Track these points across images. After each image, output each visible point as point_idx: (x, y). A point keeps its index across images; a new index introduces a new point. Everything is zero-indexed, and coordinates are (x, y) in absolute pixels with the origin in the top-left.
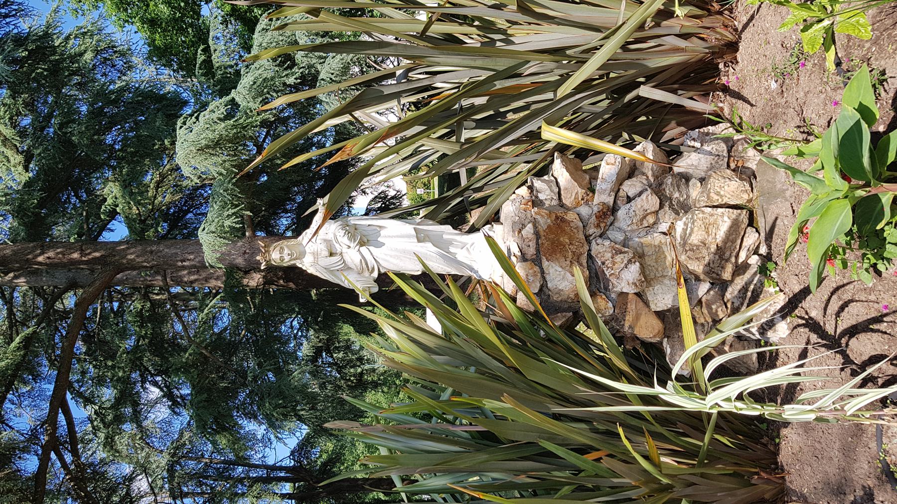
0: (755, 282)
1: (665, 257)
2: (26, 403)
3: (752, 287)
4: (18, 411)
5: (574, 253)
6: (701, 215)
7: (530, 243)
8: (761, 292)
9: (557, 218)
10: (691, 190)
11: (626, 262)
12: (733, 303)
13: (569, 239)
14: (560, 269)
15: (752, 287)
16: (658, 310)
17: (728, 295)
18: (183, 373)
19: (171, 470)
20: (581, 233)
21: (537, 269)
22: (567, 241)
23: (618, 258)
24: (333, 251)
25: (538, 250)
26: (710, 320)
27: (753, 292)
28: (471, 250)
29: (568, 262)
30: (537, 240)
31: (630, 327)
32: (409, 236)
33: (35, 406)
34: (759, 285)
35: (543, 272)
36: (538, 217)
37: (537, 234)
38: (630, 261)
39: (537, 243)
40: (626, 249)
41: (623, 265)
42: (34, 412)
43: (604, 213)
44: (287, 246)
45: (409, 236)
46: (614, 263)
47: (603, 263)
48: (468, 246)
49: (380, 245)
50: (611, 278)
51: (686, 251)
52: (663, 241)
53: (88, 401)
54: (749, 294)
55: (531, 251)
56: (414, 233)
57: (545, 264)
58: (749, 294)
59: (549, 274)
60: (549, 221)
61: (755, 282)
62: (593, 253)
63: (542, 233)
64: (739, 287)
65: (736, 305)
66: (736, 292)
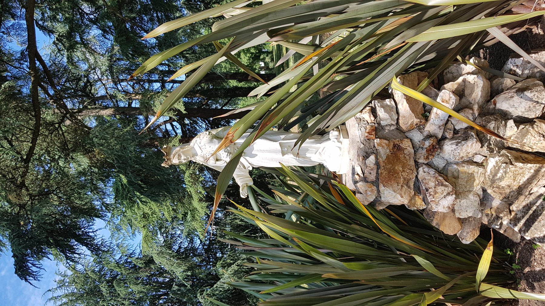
0: (538, 204)
1: (475, 180)
2: (12, 33)
3: (534, 208)
4: (9, 38)
5: (405, 179)
6: (513, 169)
7: (372, 172)
8: (541, 214)
9: (394, 146)
10: (507, 131)
11: (445, 194)
12: (516, 214)
13: (403, 167)
14: (393, 193)
15: (534, 208)
16: (461, 217)
17: (514, 207)
18: (106, 19)
19: (111, 67)
20: (412, 159)
21: (375, 188)
22: (401, 169)
23: (440, 189)
24: (219, 158)
25: (377, 178)
26: (494, 214)
27: (534, 212)
28: (322, 153)
29: (400, 187)
30: (378, 169)
31: (437, 224)
32: (274, 151)
33: (18, 34)
34: (540, 208)
35: (379, 191)
36: (380, 148)
37: (377, 164)
38: (448, 194)
39: (377, 173)
40: (447, 183)
41: (443, 195)
42: (19, 38)
43: (433, 146)
44: (183, 152)
45: (274, 151)
46: (436, 193)
47: (427, 190)
48: (320, 150)
49: (254, 156)
50: (431, 203)
51: (493, 187)
52: (475, 171)
53: (50, 32)
54: (531, 212)
55: (373, 177)
56: (279, 148)
57: (382, 188)
58: (531, 212)
59: (384, 194)
60: (388, 151)
61: (538, 204)
62: (419, 177)
63: (382, 164)
64: (524, 204)
65: (518, 216)
66: (521, 207)
